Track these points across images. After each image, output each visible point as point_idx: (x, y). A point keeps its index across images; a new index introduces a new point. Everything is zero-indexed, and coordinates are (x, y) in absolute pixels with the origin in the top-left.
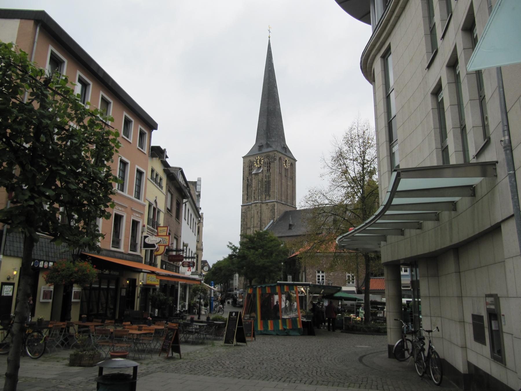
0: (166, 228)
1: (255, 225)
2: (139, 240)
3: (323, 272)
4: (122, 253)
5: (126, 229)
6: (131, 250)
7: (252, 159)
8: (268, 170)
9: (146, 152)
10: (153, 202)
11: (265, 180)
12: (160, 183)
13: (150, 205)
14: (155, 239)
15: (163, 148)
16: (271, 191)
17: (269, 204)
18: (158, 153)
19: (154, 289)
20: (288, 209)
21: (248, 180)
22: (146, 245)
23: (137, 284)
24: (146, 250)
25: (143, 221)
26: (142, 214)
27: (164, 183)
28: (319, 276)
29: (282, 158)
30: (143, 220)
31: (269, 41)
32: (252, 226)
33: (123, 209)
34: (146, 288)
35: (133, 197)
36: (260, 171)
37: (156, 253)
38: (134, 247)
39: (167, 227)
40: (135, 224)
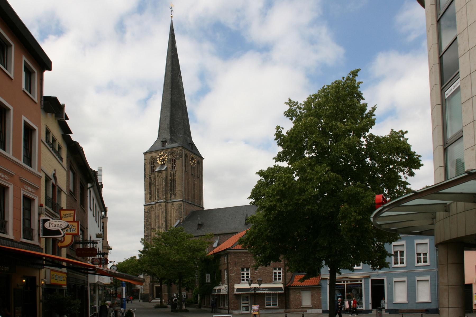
0: (73, 212)
1: (160, 225)
2: (35, 225)
3: (247, 270)
4: (11, 240)
5: (14, 207)
6: (24, 238)
7: (154, 155)
8: (173, 168)
9: (36, 100)
10: (50, 175)
11: (169, 178)
12: (58, 152)
13: (48, 179)
14: (60, 223)
15: (61, 102)
16: (177, 189)
17: (175, 203)
18: (53, 107)
19: (61, 291)
20: (196, 209)
21: (150, 178)
22: (47, 232)
23: (38, 284)
24: (46, 238)
25: (40, 199)
26: (37, 189)
27: (64, 153)
28: (243, 274)
29: (188, 155)
30: (40, 198)
31: (172, 21)
32: (157, 226)
33: (7, 177)
34: (50, 289)
35: (22, 162)
36: (164, 169)
37: (60, 244)
38: (28, 233)
39: (75, 210)
40: (28, 201)
